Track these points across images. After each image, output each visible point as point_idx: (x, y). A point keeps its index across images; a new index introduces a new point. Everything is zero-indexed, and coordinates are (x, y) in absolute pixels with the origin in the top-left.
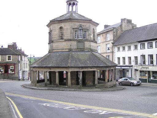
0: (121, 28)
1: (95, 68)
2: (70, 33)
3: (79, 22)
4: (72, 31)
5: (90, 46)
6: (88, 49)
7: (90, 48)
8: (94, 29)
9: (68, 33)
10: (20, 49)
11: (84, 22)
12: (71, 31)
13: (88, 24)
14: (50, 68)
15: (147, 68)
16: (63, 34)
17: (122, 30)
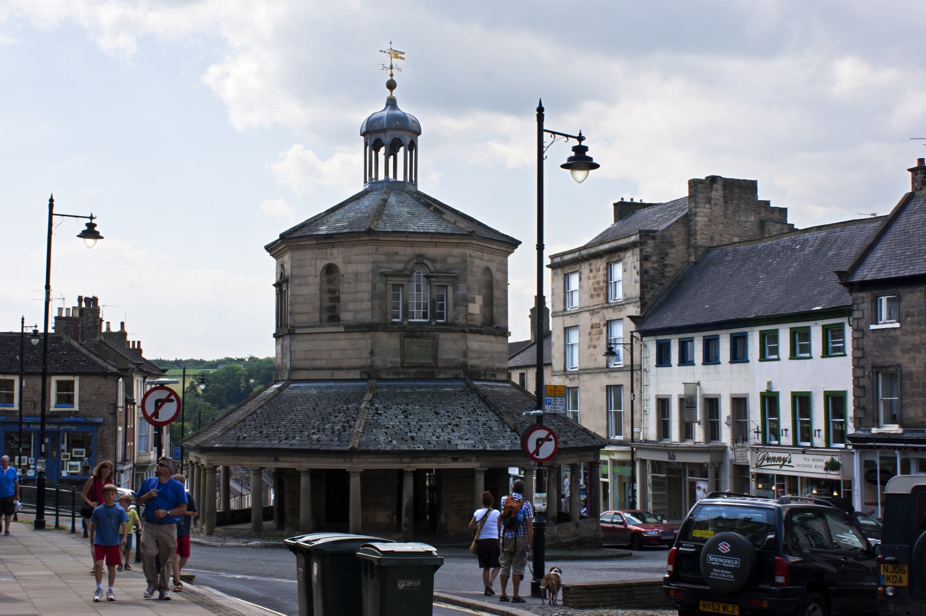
0: (690, 234)
1: (474, 459)
2: (367, 296)
3: (413, 244)
4: (380, 286)
5: (465, 354)
6: (456, 368)
7: (464, 366)
8: (488, 270)
9: (359, 295)
10: (115, 328)
11: (436, 244)
12: (374, 287)
13: (456, 251)
14: (275, 453)
15: (784, 460)
16: (337, 299)
17: (689, 245)
